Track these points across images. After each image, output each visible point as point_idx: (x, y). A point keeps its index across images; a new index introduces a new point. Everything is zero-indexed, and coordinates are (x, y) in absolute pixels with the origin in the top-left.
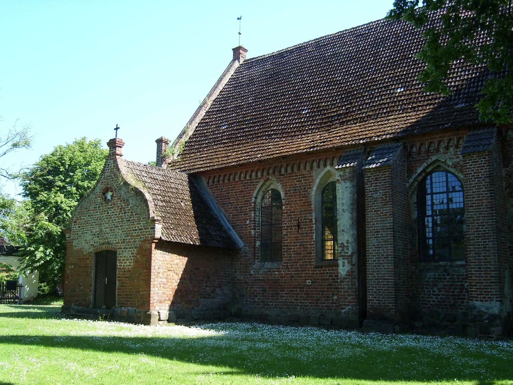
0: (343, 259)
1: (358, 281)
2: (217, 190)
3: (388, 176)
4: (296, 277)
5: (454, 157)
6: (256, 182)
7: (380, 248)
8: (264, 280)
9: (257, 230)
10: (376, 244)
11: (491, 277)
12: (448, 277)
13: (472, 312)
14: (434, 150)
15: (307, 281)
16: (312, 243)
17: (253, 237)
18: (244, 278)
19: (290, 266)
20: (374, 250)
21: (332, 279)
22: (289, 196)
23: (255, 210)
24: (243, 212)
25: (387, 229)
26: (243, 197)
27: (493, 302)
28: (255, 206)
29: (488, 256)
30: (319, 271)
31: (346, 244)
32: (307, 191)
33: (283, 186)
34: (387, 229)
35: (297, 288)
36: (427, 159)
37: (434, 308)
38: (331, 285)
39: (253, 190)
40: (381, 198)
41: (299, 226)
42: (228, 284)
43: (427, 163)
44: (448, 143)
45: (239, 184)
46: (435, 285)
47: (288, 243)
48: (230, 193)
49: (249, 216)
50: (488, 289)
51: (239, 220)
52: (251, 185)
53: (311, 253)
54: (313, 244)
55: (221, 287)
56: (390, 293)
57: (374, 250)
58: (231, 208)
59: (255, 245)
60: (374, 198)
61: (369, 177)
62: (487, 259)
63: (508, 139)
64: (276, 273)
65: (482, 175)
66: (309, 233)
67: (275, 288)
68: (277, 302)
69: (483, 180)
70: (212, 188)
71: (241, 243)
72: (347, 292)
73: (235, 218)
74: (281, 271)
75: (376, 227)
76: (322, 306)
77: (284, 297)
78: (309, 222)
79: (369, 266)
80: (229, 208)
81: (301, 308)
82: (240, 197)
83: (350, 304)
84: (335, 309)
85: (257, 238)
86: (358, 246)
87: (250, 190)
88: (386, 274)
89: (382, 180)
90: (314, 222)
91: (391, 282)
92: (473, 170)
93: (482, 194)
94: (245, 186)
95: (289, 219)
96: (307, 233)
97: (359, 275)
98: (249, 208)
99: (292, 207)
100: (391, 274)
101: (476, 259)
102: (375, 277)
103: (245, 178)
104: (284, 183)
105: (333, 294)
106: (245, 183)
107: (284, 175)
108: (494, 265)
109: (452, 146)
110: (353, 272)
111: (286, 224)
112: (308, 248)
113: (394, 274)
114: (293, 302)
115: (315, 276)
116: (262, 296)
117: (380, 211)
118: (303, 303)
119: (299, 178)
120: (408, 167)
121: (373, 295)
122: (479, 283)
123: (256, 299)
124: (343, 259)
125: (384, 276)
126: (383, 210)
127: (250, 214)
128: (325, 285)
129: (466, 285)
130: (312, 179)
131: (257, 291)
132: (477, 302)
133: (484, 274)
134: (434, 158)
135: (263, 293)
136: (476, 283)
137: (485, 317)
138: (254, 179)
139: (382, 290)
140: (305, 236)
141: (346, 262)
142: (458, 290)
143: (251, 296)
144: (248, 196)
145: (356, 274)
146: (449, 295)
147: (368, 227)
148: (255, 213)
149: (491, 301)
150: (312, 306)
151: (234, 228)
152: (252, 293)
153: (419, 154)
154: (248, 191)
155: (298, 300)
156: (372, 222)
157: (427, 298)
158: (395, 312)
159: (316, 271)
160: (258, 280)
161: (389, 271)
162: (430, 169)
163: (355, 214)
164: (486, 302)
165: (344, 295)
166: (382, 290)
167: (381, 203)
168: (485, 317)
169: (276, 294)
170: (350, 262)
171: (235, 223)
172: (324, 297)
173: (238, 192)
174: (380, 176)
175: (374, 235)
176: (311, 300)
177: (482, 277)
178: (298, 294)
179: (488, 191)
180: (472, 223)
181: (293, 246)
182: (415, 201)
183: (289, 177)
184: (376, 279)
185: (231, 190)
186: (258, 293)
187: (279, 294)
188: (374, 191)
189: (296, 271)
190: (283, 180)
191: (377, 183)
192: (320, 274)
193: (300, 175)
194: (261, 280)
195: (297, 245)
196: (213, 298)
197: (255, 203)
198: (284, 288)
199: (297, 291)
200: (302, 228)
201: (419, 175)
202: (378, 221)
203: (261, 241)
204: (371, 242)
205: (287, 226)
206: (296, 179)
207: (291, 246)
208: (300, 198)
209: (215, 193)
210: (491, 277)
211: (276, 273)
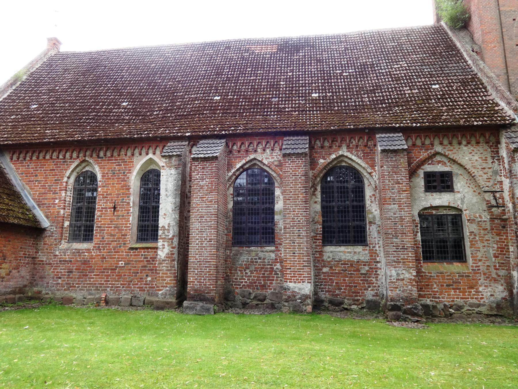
0: (163, 241)
1: (178, 262)
2: (22, 166)
3: (215, 167)
4: (108, 258)
5: (270, 157)
6: (70, 162)
7: (204, 232)
8: (71, 261)
9: (66, 210)
10: (200, 228)
11: (303, 261)
12: (260, 261)
13: (286, 292)
14: (253, 149)
15: (120, 263)
16: (128, 225)
17: (61, 217)
18: (47, 258)
19: (102, 247)
20: (197, 234)
21: (147, 261)
22: (106, 179)
23: (66, 190)
24: (52, 191)
25: (211, 215)
26: (53, 175)
27: (304, 283)
28: (66, 185)
29: (302, 243)
30: (133, 252)
31: (167, 228)
32: (126, 175)
33: (101, 168)
34: (211, 215)
35: (108, 269)
36: (246, 157)
37: (246, 288)
38: (145, 267)
39: (67, 170)
40: (207, 186)
41: (115, 208)
42: (27, 266)
43: (245, 160)
44: (266, 145)
45: (50, 162)
46: (248, 268)
47: (101, 224)
48: (38, 170)
49: (58, 196)
50: (301, 272)
51: (47, 199)
52: (64, 165)
53: (126, 235)
54: (129, 227)
55: (18, 268)
56: (211, 274)
57: (197, 234)
58: (38, 186)
59: (63, 225)
60: (200, 186)
61: (196, 166)
62: (403, 241)
63: (316, 147)
64: (86, 254)
65: (299, 173)
66: (126, 216)
67: (83, 270)
68: (85, 284)
69: (300, 178)
70: (17, 164)
71: (45, 223)
72: (166, 274)
73: (42, 196)
74: (92, 252)
75: (201, 212)
76: (135, 287)
77: (93, 278)
78: (126, 205)
79: (192, 249)
80: (35, 186)
81: (111, 290)
82: (50, 175)
83: (168, 286)
84: (148, 291)
85: (66, 218)
86: (179, 230)
87: (62, 170)
88: (208, 257)
89: (209, 170)
90: (131, 205)
91: (213, 264)
92: (291, 169)
93: (298, 189)
94: (57, 164)
95: (105, 201)
96: (123, 216)
97: (178, 257)
98: (60, 188)
99: (109, 189)
100: (213, 257)
101: (292, 246)
102: (197, 259)
103: (58, 157)
104: (102, 166)
105: (147, 276)
106: (57, 162)
107: (102, 158)
108: (306, 251)
109: (268, 148)
110: (173, 254)
111: (101, 205)
112: (123, 230)
113: (216, 257)
114: (103, 284)
115: (129, 258)
116: (67, 278)
117: (205, 197)
118: (114, 284)
119: (119, 162)
120: (228, 162)
121: (195, 277)
122: (293, 266)
123: (60, 280)
124: (163, 241)
125: (206, 259)
126: (208, 197)
127: (60, 193)
128: (139, 267)
129: (275, 268)
130: (133, 164)
131: (61, 272)
132: (290, 284)
133: (297, 259)
134: (252, 157)
135: (69, 275)
136: (291, 266)
137: (297, 297)
138: (68, 159)
139: (203, 272)
140: (121, 219)
141: (166, 244)
142: (268, 273)
143: (53, 278)
144: (59, 175)
145: (176, 256)
146: (260, 277)
147: (193, 212)
148: (66, 193)
149: (303, 282)
150: (123, 287)
151: (39, 207)
152: (55, 275)
153: (239, 151)
154: (60, 170)
155: (109, 281)
156: (197, 207)
157: (240, 279)
158: (216, 293)
159: (130, 252)
160: (63, 261)
161: (211, 254)
162: (247, 166)
163: (178, 200)
164: (299, 284)
165: (162, 277)
166: (203, 272)
167: (206, 190)
168: (297, 297)
169: (83, 275)
170: (171, 245)
171: (41, 202)
172: (137, 279)
173: (48, 170)
174: (207, 166)
175: (198, 220)
176: (123, 281)
177: (296, 261)
178: (110, 275)
179: (304, 187)
180: (288, 214)
181: (107, 227)
182: (232, 193)
183: (108, 160)
184: (198, 262)
185: (39, 168)
186: (62, 275)
187: (87, 275)
188: (200, 179)
189: (109, 252)
190: (101, 163)
191: (203, 172)
192: (135, 255)
193: (120, 160)
194: (68, 261)
195: (111, 227)
196: (9, 281)
197: (67, 183)
198: (94, 269)
199: (108, 272)
200: (118, 211)
201: (238, 170)
202: (202, 207)
203: (70, 221)
204: (195, 225)
205: (102, 208)
206: (115, 163)
207: (104, 227)
208: (118, 181)
209: (19, 169)
210: (303, 261)
211: (86, 254)
